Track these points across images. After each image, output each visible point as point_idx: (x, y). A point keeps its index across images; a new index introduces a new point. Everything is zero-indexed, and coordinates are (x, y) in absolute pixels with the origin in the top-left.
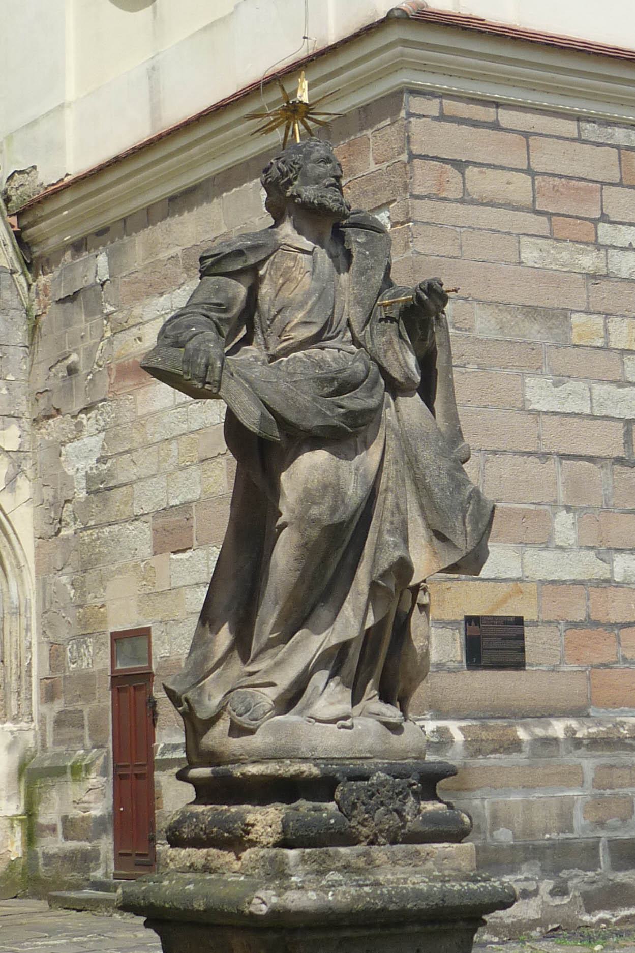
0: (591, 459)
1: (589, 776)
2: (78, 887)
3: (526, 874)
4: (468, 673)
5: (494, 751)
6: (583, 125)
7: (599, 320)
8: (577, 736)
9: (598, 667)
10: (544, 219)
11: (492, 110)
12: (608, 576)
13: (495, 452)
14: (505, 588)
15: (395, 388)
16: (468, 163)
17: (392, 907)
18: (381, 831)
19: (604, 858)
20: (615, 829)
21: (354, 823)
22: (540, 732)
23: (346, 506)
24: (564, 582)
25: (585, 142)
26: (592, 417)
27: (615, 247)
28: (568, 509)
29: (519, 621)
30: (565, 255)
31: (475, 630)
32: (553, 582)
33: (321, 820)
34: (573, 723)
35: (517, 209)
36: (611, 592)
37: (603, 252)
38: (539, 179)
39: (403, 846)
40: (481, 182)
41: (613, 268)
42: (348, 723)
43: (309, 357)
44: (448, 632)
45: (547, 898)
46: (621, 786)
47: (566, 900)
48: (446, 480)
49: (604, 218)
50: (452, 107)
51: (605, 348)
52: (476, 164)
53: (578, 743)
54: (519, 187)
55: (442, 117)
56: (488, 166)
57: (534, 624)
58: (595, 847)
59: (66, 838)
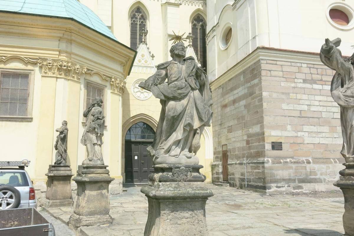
0: (294, 117)
1: (294, 168)
2: (218, 182)
3: (283, 183)
4: (272, 151)
5: (277, 163)
6: (292, 63)
7: (295, 94)
8: (292, 161)
9: (295, 150)
10: (285, 79)
11: (276, 62)
12: (297, 135)
13: (277, 116)
14: (279, 137)
15: (193, 89)
16: (272, 70)
17: (181, 195)
18: (182, 179)
19: (297, 181)
20: (299, 177)
21: (175, 177)
22: (285, 160)
23: (177, 112)
24: (289, 136)
25: (292, 66)
26: (294, 110)
27: (298, 83)
28: (290, 125)
29: (281, 143)
30: (289, 84)
31: (273, 144)
32: (287, 136)
33: (167, 176)
34: (291, 159)
35: (280, 77)
36: (298, 138)
37: (295, 84)
38: (284, 72)
39: (187, 182)
40: (273, 73)
41: (297, 86)
42: (177, 156)
43: (175, 84)
44: (269, 144)
45: (287, 188)
46: (300, 170)
47: (290, 188)
48: (203, 107)
49: (296, 78)
50: (268, 61)
51: (296, 99)
52: (273, 70)
53: (292, 163)
54: (281, 74)
55: (267, 63)
56: (275, 71)
57: (284, 143)
58: (295, 179)
59: (216, 175)
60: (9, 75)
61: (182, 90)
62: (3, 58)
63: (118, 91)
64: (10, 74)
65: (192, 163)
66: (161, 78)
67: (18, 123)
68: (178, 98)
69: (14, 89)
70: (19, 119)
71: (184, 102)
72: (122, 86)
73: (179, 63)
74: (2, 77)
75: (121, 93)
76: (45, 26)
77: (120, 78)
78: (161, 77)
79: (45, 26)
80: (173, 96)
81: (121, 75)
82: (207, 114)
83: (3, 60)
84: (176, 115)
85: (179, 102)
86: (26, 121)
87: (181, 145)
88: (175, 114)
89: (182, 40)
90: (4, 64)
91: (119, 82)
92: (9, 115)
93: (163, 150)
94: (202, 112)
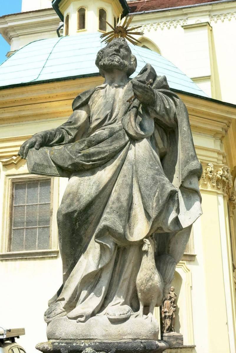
42: (83, 319)
60: (24, 184)
61: (101, 145)
62: (13, 159)
63: (213, 186)
64: (24, 182)
65: (126, 337)
66: (78, 128)
67: (38, 262)
68: (86, 168)
69: (31, 206)
70: (39, 255)
71: (104, 175)
72: (221, 176)
73: (110, 85)
74: (14, 189)
75: (222, 189)
76: (68, 95)
77: (216, 160)
78: (75, 126)
79: (68, 95)
80: (71, 165)
81: (216, 155)
82: (158, 197)
83: (13, 161)
84: (75, 211)
85: (92, 177)
86: (49, 257)
87: (101, 287)
88: (72, 208)
89: (131, 35)
90: (15, 168)
91: (213, 169)
92: (26, 249)
93: (62, 302)
94: (148, 193)
